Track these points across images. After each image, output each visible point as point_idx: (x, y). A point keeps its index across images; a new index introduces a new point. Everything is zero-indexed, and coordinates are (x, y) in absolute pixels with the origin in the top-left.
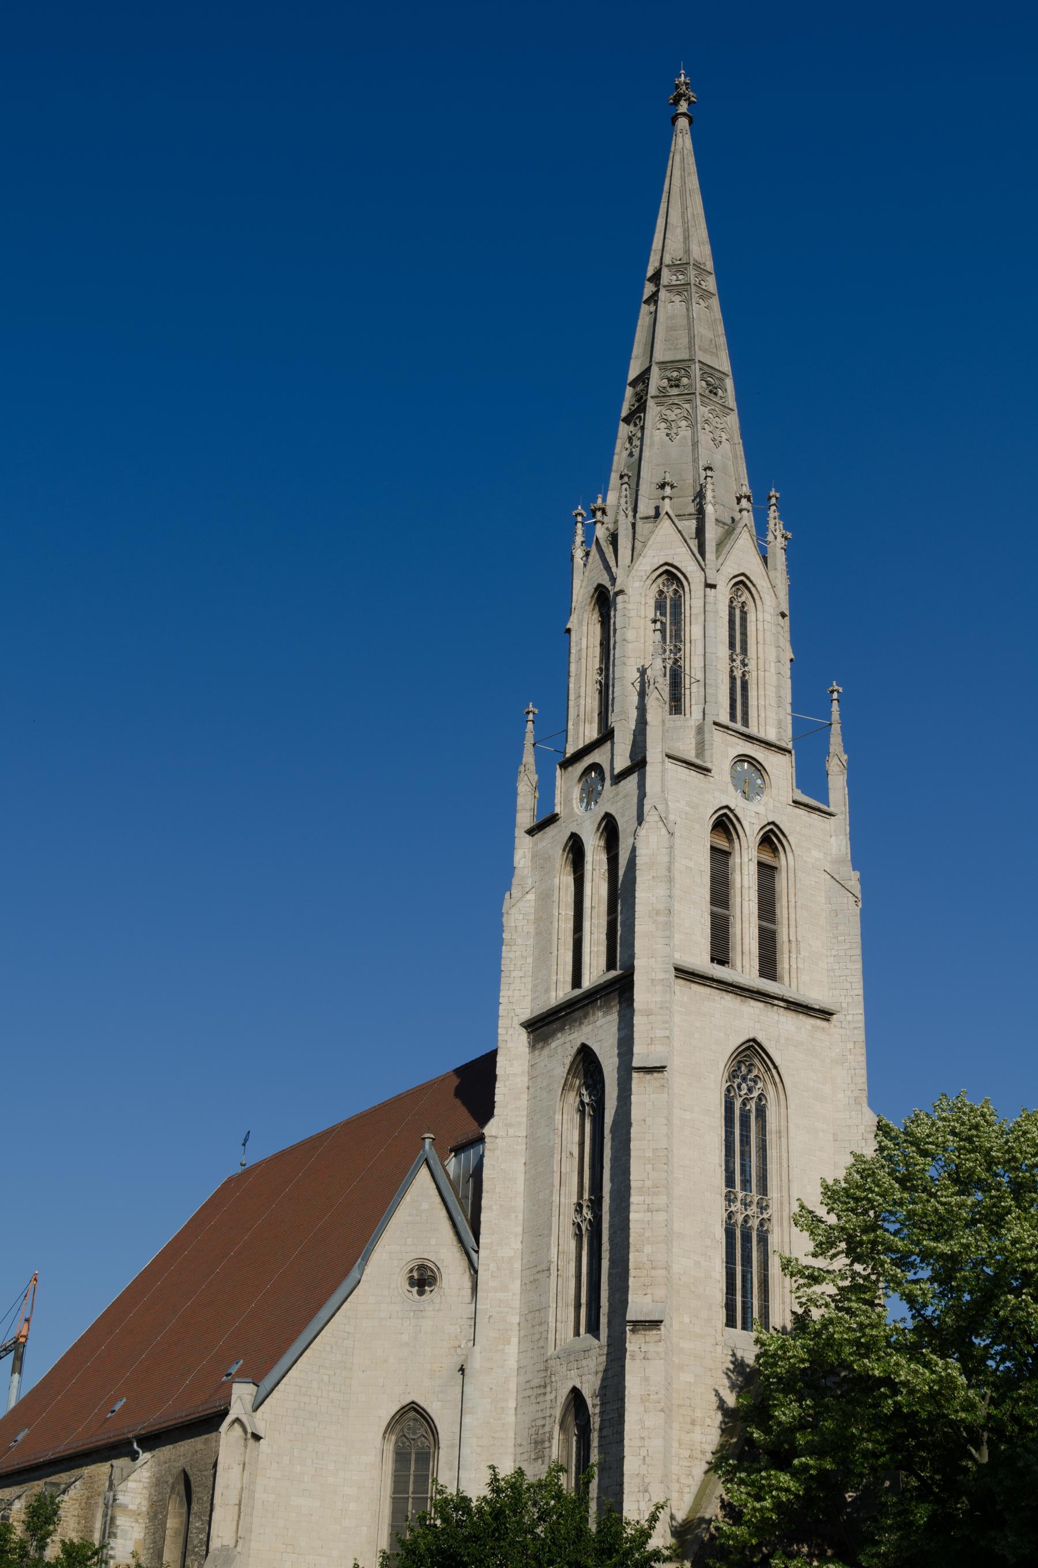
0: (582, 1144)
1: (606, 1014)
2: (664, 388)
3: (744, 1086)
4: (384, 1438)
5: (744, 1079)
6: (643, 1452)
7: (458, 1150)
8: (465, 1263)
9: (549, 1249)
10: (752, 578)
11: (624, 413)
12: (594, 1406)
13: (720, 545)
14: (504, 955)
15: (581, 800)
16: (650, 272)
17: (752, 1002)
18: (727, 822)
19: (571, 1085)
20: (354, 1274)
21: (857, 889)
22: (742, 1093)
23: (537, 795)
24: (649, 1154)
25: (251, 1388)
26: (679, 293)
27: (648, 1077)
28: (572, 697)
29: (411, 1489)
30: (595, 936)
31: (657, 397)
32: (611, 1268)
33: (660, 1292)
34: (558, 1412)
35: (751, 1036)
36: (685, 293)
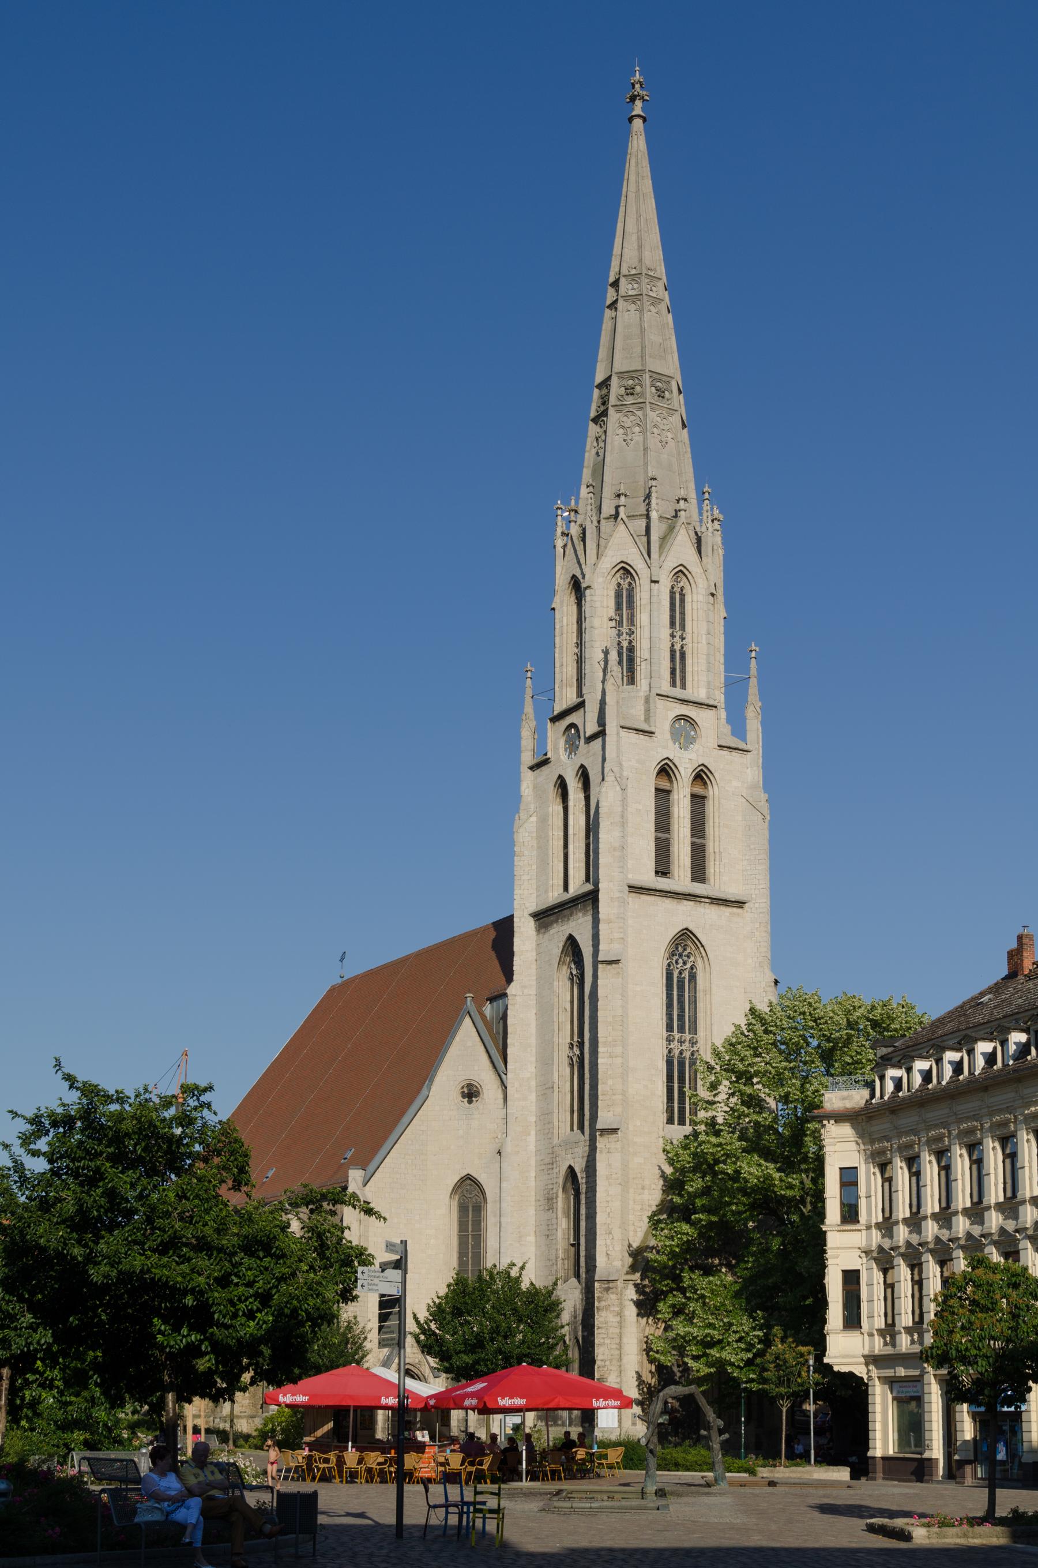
0: (572, 1002)
1: (584, 914)
2: (622, 396)
3: (680, 961)
4: (451, 1197)
5: (681, 956)
6: (608, 1210)
7: (492, 1000)
8: (498, 1082)
9: (553, 1074)
10: (688, 567)
11: (593, 414)
12: (582, 1178)
13: (664, 539)
14: (516, 863)
15: (566, 750)
16: (611, 279)
17: (685, 902)
18: (668, 769)
19: (564, 962)
20: (424, 1092)
21: (766, 811)
22: (678, 966)
23: (536, 737)
24: (610, 1019)
25: (361, 1173)
26: (634, 303)
27: (609, 967)
28: (557, 665)
29: (470, 1230)
30: (577, 855)
31: (616, 406)
32: (590, 1090)
33: (618, 1110)
34: (561, 1181)
35: (684, 927)
36: (638, 302)
